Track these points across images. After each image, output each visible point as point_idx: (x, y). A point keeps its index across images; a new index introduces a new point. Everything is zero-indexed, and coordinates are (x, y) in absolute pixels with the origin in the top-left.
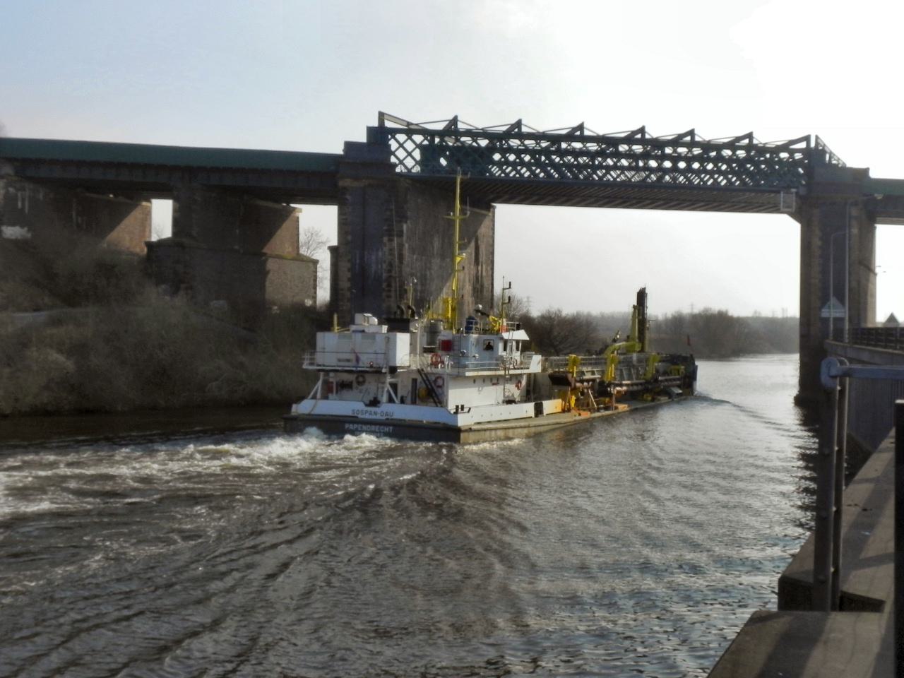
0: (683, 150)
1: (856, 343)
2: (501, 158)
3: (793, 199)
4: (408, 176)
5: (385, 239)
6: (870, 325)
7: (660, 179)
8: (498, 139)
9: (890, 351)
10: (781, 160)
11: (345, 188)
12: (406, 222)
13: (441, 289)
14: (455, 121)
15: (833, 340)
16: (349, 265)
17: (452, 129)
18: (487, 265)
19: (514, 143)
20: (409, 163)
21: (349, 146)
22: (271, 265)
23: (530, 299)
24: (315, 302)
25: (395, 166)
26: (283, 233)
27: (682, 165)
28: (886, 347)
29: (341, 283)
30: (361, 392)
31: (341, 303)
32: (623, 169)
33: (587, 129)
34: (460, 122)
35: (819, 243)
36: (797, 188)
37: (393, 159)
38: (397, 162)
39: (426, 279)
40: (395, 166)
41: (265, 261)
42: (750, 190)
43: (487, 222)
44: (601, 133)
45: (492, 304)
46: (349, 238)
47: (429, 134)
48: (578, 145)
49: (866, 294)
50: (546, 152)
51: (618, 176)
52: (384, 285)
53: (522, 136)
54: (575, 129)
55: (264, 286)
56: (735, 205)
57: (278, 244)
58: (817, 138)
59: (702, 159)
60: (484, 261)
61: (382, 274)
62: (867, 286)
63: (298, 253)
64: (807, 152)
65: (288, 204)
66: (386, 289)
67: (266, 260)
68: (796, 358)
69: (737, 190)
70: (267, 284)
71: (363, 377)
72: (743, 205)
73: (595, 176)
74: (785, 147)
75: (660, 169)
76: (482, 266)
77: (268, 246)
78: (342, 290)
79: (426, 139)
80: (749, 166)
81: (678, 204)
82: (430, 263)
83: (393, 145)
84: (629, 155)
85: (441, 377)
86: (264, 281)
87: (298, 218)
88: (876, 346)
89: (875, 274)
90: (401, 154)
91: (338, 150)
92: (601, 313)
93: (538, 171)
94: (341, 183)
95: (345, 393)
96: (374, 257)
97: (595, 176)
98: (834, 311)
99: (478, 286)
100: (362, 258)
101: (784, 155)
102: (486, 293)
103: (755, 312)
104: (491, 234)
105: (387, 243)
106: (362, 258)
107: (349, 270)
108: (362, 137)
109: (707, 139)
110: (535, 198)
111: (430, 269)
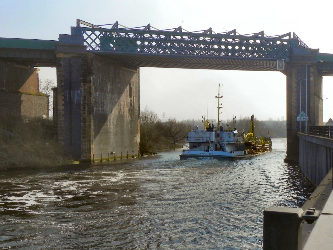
0: (230, 40)
1: (311, 134)
2: (152, 43)
3: (283, 65)
4: (93, 52)
5: (82, 84)
6: (320, 125)
7: (226, 55)
8: (139, 33)
9: (326, 138)
10: (277, 45)
11: (60, 59)
12: (92, 76)
13: (112, 110)
14: (149, 26)
15: (301, 132)
16: (63, 98)
17: (115, 28)
18: (136, 97)
19: (147, 36)
20: (93, 45)
21: (62, 36)
22: (23, 97)
23: (165, 114)
24: (48, 116)
25: (86, 47)
26: (30, 81)
27: (230, 47)
28: (324, 136)
29: (59, 107)
30: (199, 148)
31: (59, 117)
32: (201, 49)
33: (237, 33)
34: (237, 33)
35: (296, 85)
36: (285, 58)
37: (85, 43)
38: (87, 45)
39: (104, 104)
40: (86, 47)
41: (20, 96)
42: (263, 60)
43: (135, 75)
44: (190, 31)
45: (139, 116)
46: (63, 84)
47: (106, 31)
48: (179, 37)
49: (318, 109)
50: (164, 41)
51: (213, 53)
52: (82, 108)
53: (182, 34)
54: (206, 31)
55: (20, 109)
56: (256, 67)
57: (27, 87)
58: (294, 33)
59: (240, 45)
60: (134, 95)
61: (80, 102)
62: (318, 106)
63: (38, 92)
64: (289, 41)
65: (32, 67)
66: (83, 109)
67: (21, 95)
68: (285, 139)
69: (257, 59)
70: (22, 107)
71: (200, 144)
72: (260, 67)
73: (195, 53)
74: (280, 38)
75: (220, 49)
76: (133, 98)
77: (21, 88)
78: (60, 110)
79: (102, 33)
80: (190, 44)
81: (223, 67)
82: (106, 96)
83: (85, 36)
84: (205, 42)
85: (223, 144)
86: (20, 106)
87: (38, 74)
88: (320, 135)
89: (322, 100)
90: (89, 41)
91: (56, 38)
92: (199, 120)
93: (167, 50)
94: (58, 56)
95: (195, 148)
96: (76, 94)
97: (195, 53)
98: (303, 118)
99: (132, 108)
100: (70, 93)
101: (278, 42)
102: (136, 111)
103: (270, 118)
104: (138, 82)
105: (83, 86)
106: (70, 93)
107: (63, 100)
108: (69, 32)
109: (269, 36)
110: (159, 64)
111: (106, 99)
